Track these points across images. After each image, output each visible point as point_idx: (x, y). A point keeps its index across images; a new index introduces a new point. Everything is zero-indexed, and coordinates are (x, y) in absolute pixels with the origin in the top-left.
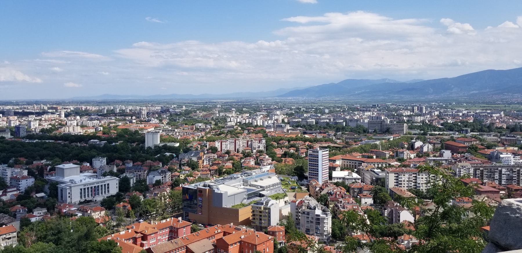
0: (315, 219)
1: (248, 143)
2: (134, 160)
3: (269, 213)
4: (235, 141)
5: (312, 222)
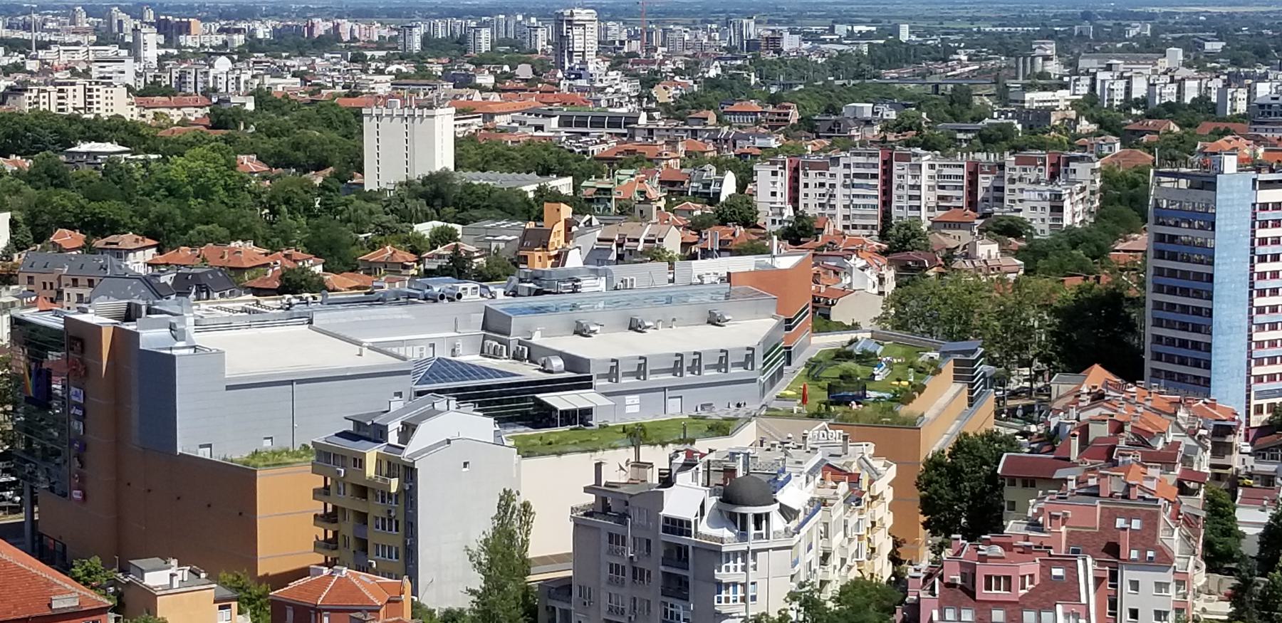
0: (659, 552)
1: (973, 183)
2: (162, 235)
3: (409, 496)
4: (887, 164)
5: (639, 574)
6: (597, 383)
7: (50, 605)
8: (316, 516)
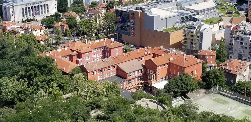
3: (201, 37)
5: (245, 48)
6: (200, 14)
7: (169, 60)
8: (183, 36)
